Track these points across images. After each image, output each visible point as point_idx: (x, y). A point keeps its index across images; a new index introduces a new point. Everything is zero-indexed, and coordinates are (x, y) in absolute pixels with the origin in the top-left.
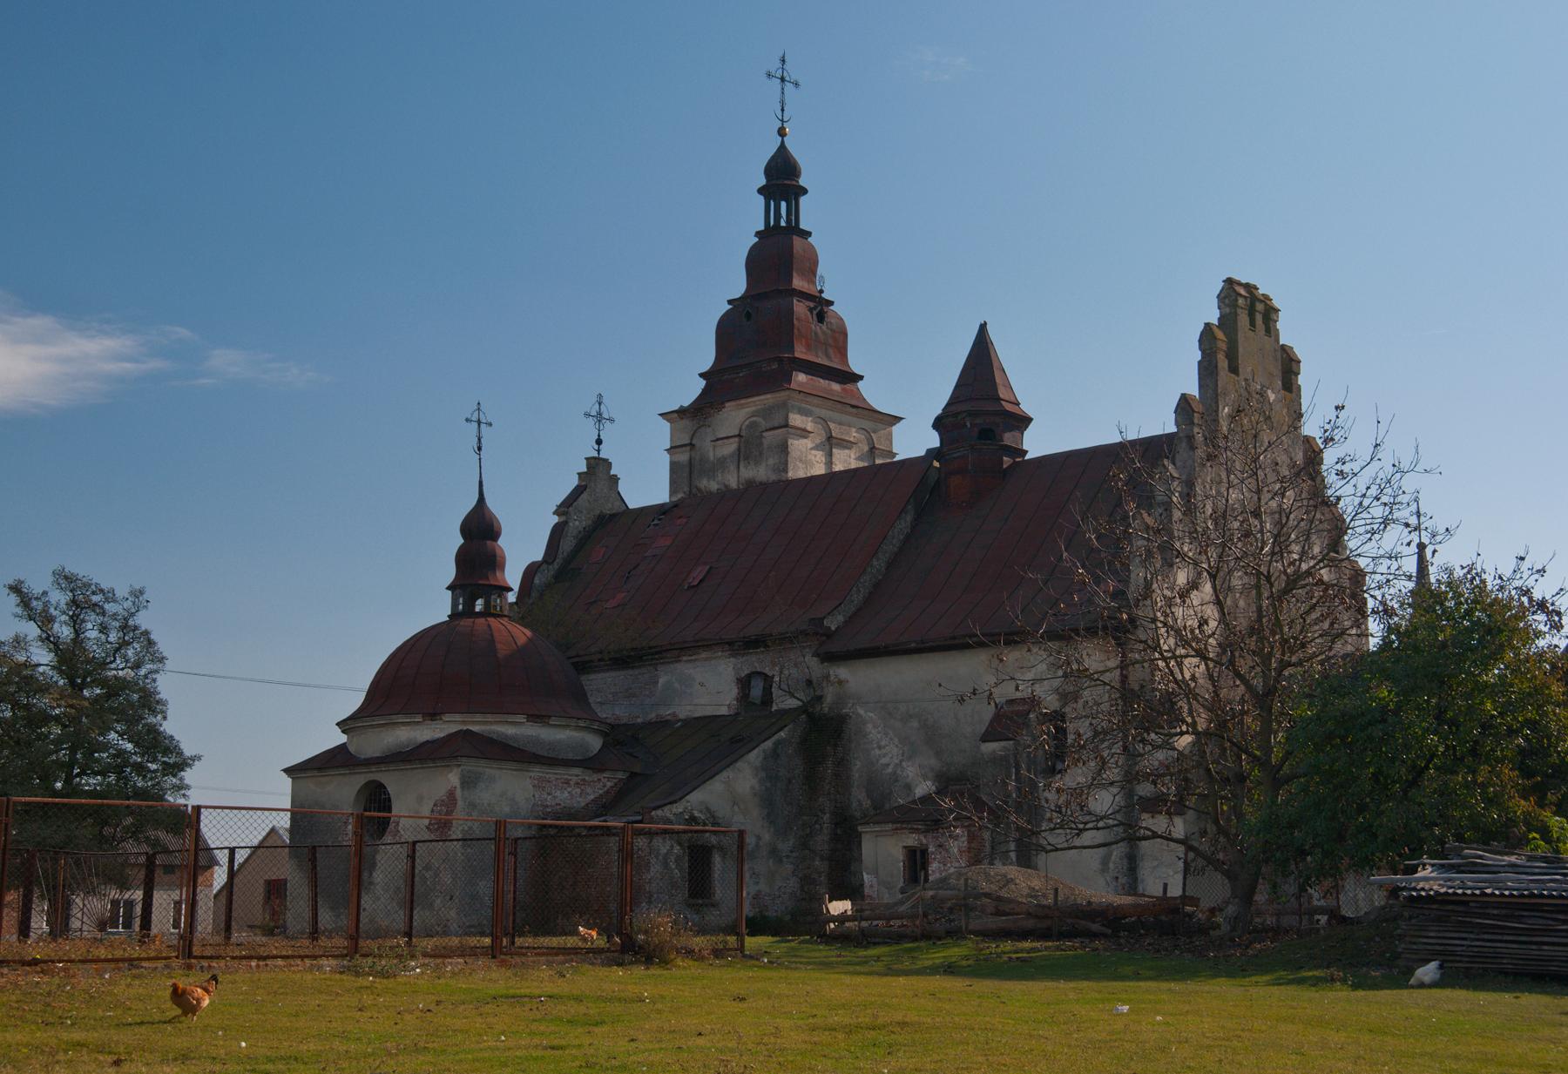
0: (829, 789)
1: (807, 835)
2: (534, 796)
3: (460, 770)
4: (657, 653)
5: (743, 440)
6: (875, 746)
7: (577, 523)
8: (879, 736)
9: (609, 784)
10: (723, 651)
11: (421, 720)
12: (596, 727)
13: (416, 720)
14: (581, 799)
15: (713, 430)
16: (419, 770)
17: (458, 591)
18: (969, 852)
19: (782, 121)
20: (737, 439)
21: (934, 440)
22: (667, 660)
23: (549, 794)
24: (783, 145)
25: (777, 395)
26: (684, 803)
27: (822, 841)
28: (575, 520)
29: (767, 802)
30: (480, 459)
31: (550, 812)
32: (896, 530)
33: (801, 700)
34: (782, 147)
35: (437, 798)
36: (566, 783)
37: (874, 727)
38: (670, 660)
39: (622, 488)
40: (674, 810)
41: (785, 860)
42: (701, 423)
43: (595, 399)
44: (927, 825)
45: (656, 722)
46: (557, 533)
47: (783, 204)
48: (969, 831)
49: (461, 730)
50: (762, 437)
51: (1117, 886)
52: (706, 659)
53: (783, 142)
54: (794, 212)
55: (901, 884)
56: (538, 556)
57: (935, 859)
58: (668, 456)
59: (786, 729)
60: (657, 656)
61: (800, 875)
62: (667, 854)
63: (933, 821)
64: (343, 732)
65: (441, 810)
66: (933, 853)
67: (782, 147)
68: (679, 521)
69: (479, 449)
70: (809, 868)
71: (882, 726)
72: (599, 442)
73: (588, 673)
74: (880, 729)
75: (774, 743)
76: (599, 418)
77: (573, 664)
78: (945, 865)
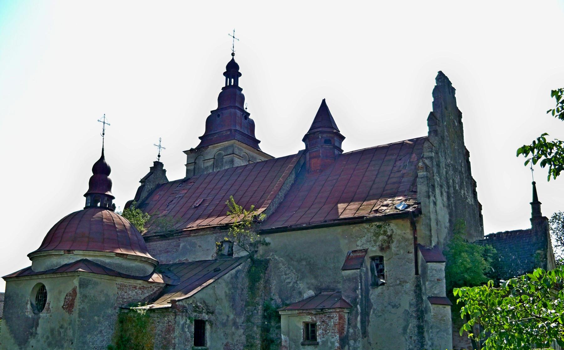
0: (262, 294)
1: (250, 315)
2: (118, 293)
3: (79, 278)
6: (284, 273)
8: (286, 269)
11: (63, 253)
12: (150, 262)
14: (142, 296)
16: (60, 278)
17: (89, 197)
18: (339, 325)
20: (213, 160)
22: (184, 236)
23: (126, 292)
24: (233, 59)
25: (230, 142)
29: (232, 299)
31: (125, 301)
32: (288, 181)
35: (68, 292)
36: (134, 288)
39: (167, 175)
40: (188, 302)
41: (240, 327)
42: (199, 154)
43: (159, 139)
44: (317, 311)
45: (178, 263)
46: (140, 190)
47: (232, 80)
48: (339, 315)
49: (83, 259)
50: (223, 158)
52: (202, 235)
53: (233, 58)
54: (236, 82)
55: (302, 340)
56: (132, 197)
57: (320, 328)
59: (241, 265)
60: (180, 234)
61: (246, 334)
62: (183, 324)
64: (31, 259)
65: (69, 298)
66: (319, 325)
68: (190, 184)
69: (103, 134)
71: (287, 264)
72: (159, 156)
73: (149, 242)
74: (286, 265)
75: (236, 271)
76: (160, 147)
77: (143, 237)
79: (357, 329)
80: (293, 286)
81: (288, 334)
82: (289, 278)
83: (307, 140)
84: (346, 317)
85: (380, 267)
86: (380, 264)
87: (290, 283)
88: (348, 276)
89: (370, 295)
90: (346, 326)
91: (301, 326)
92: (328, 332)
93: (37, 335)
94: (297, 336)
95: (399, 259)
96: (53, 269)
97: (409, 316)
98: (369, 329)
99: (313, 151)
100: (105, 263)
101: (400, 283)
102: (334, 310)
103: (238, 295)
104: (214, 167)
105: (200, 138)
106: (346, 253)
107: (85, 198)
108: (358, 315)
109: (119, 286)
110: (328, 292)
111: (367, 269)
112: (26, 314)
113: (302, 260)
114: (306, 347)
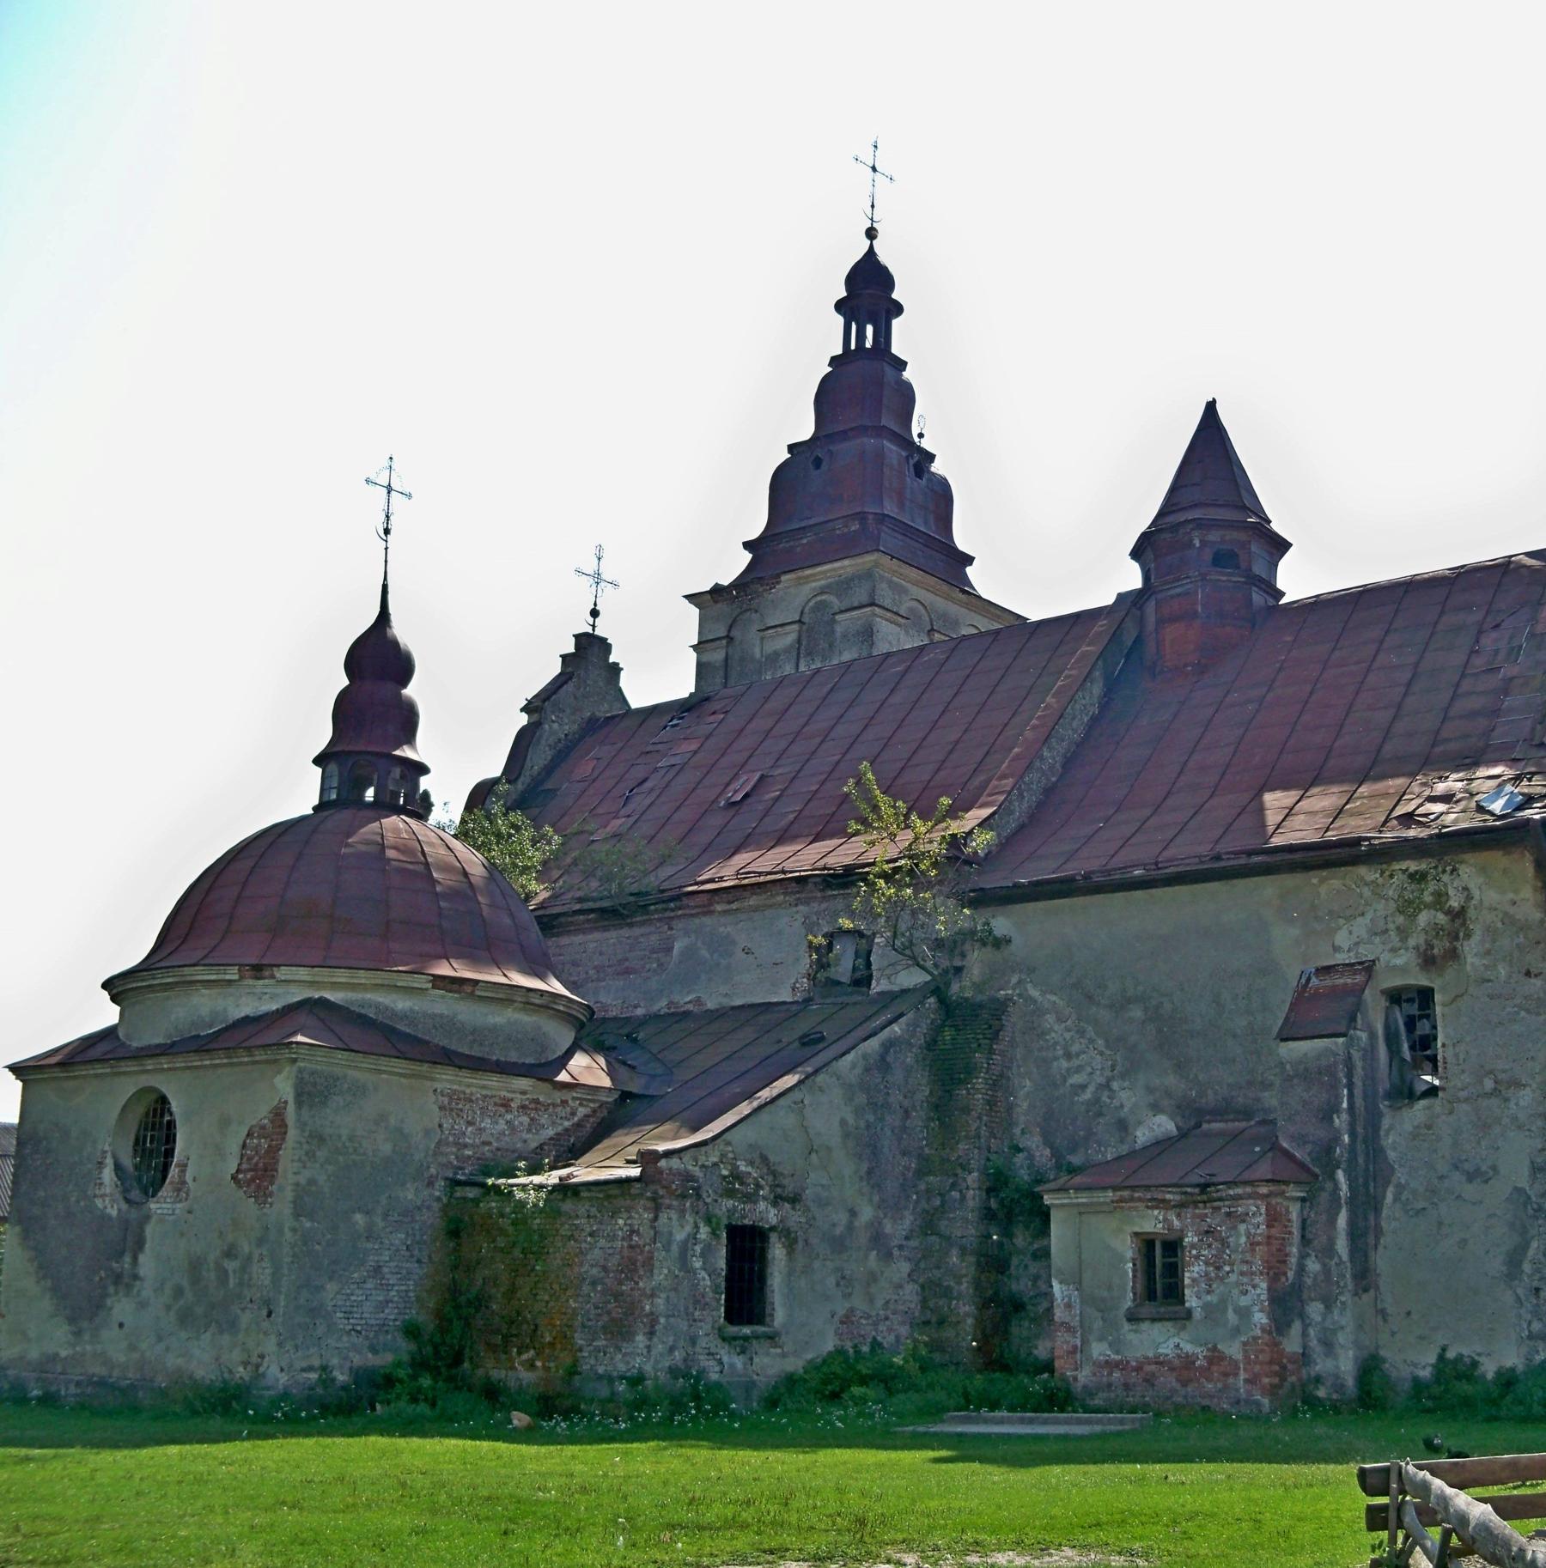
1: (936, 1209)
2: (440, 1126)
4: (672, 899)
5: (805, 627)
6: (1061, 1052)
7: (555, 726)
8: (1068, 1036)
9: (582, 1111)
10: (785, 894)
11: (236, 977)
12: (561, 1008)
13: (228, 977)
15: (761, 615)
18: (1268, 1244)
19: (872, 219)
21: (1131, 578)
22: (687, 912)
23: (469, 1123)
25: (859, 560)
26: (722, 1147)
27: (964, 1223)
28: (553, 721)
29: (867, 1147)
30: (386, 549)
31: (469, 1157)
32: (1077, 706)
33: (930, 973)
34: (871, 252)
35: (254, 1122)
36: (503, 1105)
37: (1060, 1020)
38: (693, 912)
40: (702, 1160)
41: (896, 1252)
43: (594, 551)
46: (523, 741)
47: (869, 329)
49: (310, 998)
50: (833, 621)
51: (1537, 1305)
53: (871, 247)
54: (884, 336)
55: (1128, 1302)
56: (495, 769)
57: (1197, 1257)
58: (695, 654)
60: (672, 905)
61: (921, 1280)
63: (1198, 1185)
64: (114, 999)
65: (259, 1145)
66: (1193, 1246)
67: (871, 252)
68: (712, 719)
69: (387, 531)
70: (938, 1268)
71: (1074, 1017)
72: (595, 613)
73: (558, 935)
75: (883, 1045)
76: (598, 578)
78: (1218, 1268)
79: (1336, 1259)
80: (1096, 1100)
81: (1075, 1279)
82: (1079, 1069)
83: (1149, 555)
84: (1294, 1216)
85: (1423, 1028)
86: (1421, 1017)
87: (1083, 1087)
88: (1301, 1062)
89: (1382, 1133)
90: (1295, 1250)
91: (1127, 1249)
92: (1228, 1273)
93: (138, 1283)
94: (1110, 1288)
95: (1491, 997)
96: (198, 1036)
97: (1531, 1212)
98: (1381, 1261)
99: (1172, 592)
100: (394, 1014)
101: (1495, 1089)
102: (1249, 1190)
103: (889, 1133)
104: (799, 654)
105: (748, 545)
106: (1292, 976)
107: (319, 770)
108: (1339, 1207)
109: (446, 1100)
110: (1226, 1121)
111: (1373, 1036)
112: (99, 1203)
113: (1129, 1001)
114: (1145, 1326)
